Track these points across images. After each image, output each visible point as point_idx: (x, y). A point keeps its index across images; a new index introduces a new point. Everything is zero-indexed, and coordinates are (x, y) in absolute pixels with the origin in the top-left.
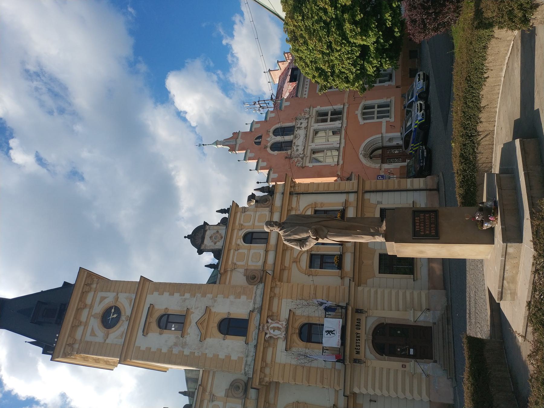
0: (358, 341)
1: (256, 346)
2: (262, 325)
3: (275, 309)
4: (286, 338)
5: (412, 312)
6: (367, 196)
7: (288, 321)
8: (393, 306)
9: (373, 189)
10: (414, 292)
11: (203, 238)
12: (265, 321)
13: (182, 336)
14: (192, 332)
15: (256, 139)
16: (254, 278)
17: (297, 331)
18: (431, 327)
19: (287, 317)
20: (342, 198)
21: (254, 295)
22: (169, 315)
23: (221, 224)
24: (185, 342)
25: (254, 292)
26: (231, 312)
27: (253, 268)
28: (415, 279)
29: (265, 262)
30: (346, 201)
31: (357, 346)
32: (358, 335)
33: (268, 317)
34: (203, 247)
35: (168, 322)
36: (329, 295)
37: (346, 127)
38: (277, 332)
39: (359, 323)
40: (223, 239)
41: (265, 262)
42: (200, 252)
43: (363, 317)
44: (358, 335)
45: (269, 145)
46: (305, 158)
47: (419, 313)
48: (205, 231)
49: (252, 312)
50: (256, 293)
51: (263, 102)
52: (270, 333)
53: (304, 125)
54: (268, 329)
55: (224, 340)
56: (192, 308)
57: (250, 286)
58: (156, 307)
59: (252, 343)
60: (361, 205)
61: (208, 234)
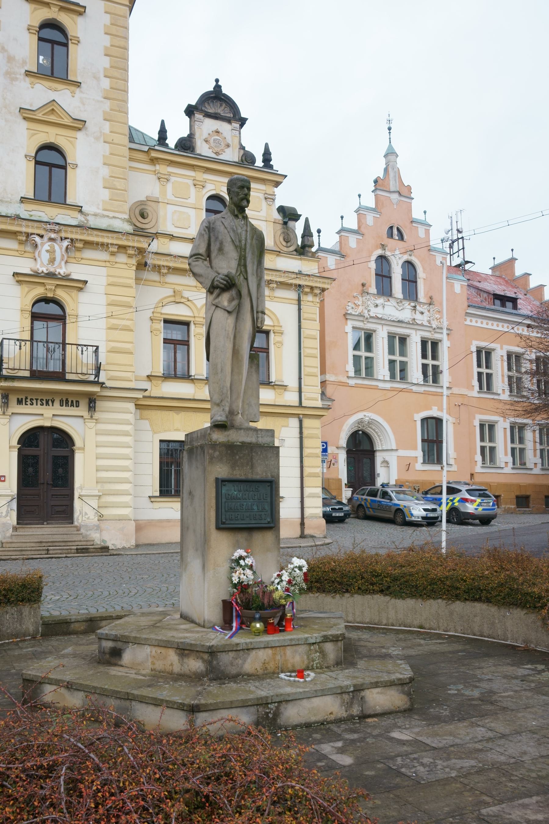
0: (39, 402)
1: (18, 217)
2: (57, 228)
3: (89, 254)
4: (36, 274)
5: (96, 493)
6: (294, 423)
7: (66, 278)
8: (101, 462)
9: (305, 432)
10: (130, 497)
11: (215, 117)
12: (63, 235)
13: (28, 73)
14: (39, 94)
15: (398, 229)
16: (143, 215)
17: (50, 295)
18: (72, 523)
19: (74, 276)
20: (291, 381)
21: (111, 214)
22: (66, 45)
23: (242, 152)
24: (16, 79)
25: (117, 215)
26: (78, 170)
27: (161, 213)
28: (153, 500)
29: (172, 237)
30: (284, 387)
31: (31, 400)
32: (50, 403)
33: (72, 240)
34: (198, 116)
35: (53, 43)
36: (312, 438)
37: (411, 391)
38: (45, 257)
39: (72, 405)
40: (214, 156)
41: (172, 237)
42: (190, 111)
43: (82, 410)
44: (50, 403)
45: (388, 253)
46: (361, 319)
47: (94, 503)
48: (229, 121)
49: (79, 209)
50: (114, 217)
51: (461, 247)
52: (43, 244)
53: (418, 316)
54: (51, 239)
55: (26, 156)
56: (81, 92)
57: (126, 207)
58: (80, 20)
59: (23, 211)
60: (281, 412)
61: (224, 127)
